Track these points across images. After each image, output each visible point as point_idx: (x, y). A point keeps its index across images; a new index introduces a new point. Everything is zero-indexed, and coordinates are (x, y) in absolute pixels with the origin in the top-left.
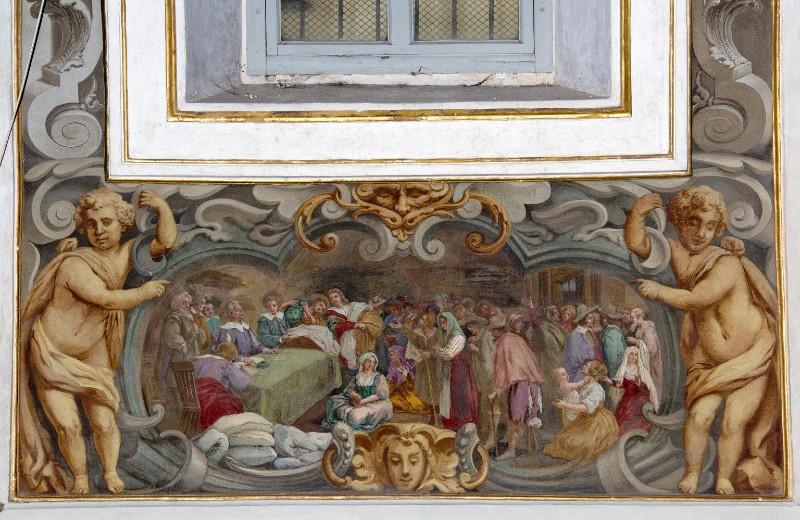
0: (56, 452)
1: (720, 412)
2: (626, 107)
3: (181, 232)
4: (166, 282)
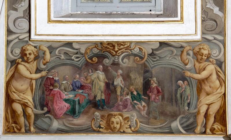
3: (51, 57)
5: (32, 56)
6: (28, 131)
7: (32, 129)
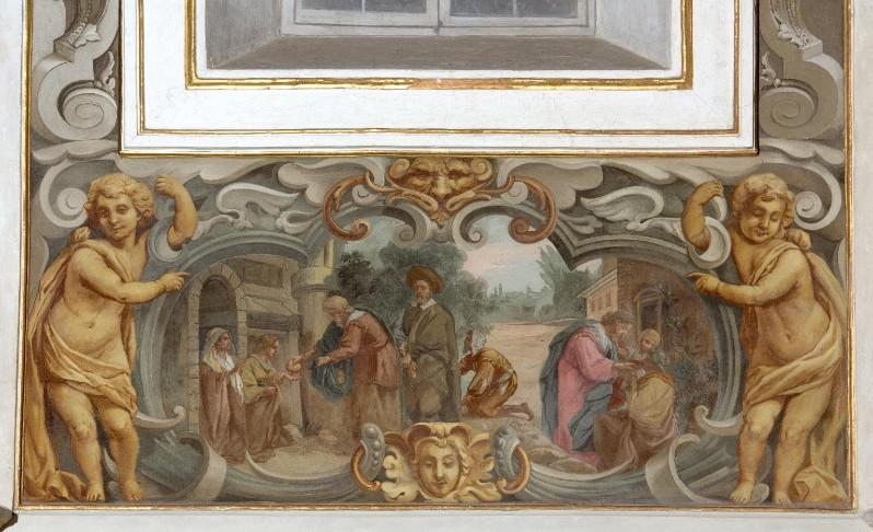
0: (69, 460)
2: (686, 81)
5: (131, 217)
6: (113, 496)
7: (132, 485)
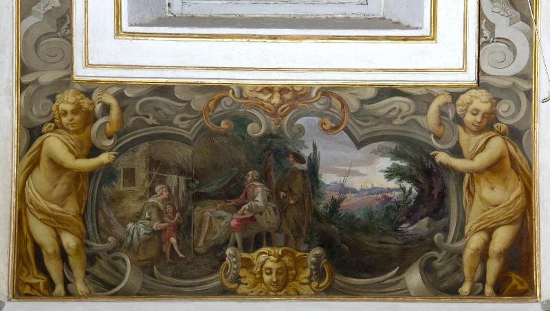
1: (487, 244)
2: (432, 38)
4: (115, 153)
